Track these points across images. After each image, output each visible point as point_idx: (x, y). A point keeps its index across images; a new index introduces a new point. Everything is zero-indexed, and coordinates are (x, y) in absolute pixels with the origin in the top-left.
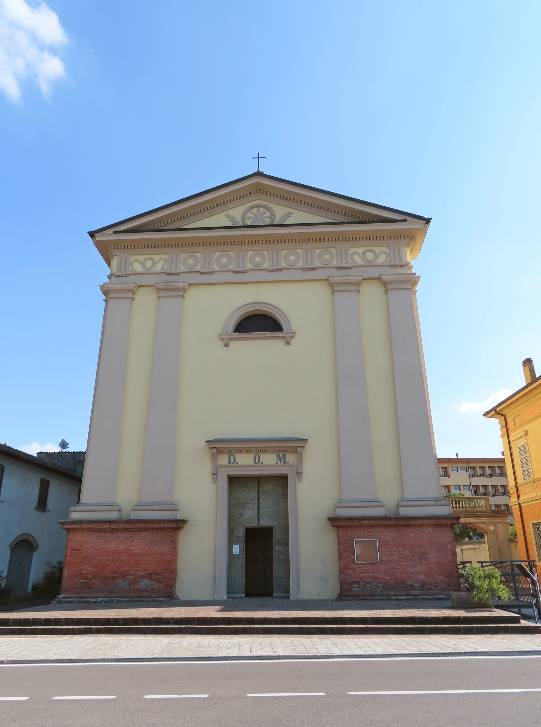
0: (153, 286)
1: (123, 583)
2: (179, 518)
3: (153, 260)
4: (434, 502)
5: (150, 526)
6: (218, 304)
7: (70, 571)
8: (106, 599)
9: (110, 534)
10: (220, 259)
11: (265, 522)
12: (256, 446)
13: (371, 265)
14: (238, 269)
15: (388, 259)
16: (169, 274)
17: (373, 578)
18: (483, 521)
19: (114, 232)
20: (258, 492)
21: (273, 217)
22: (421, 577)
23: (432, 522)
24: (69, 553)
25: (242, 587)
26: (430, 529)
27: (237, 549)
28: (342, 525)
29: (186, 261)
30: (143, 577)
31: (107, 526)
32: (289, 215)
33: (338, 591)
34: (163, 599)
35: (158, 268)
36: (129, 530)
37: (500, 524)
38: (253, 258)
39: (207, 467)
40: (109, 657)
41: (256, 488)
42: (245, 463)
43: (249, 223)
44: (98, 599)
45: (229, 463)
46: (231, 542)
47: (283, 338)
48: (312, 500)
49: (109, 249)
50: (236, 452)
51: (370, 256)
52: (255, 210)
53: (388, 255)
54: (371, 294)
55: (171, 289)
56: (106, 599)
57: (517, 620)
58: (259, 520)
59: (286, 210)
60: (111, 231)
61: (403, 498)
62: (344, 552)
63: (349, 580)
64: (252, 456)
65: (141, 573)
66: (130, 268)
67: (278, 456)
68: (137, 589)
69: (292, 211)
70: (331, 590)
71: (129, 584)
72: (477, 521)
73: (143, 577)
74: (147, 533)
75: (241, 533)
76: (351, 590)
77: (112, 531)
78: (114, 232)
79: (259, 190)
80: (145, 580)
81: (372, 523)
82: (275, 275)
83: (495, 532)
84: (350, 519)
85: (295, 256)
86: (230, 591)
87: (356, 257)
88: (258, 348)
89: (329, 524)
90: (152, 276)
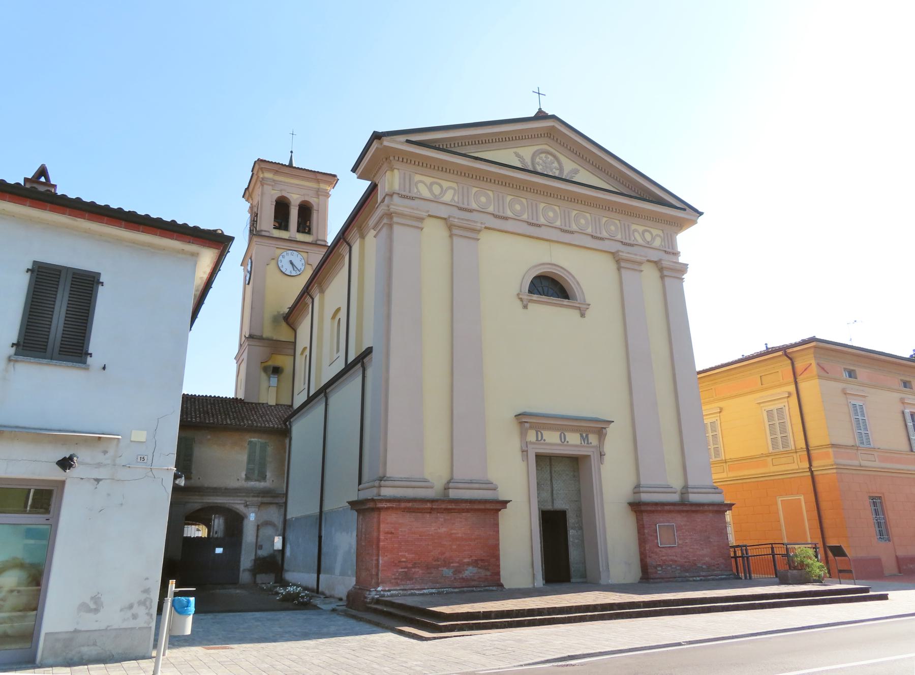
1: (447, 572)
5: (476, 507)
6: (524, 257)
7: (386, 558)
8: (434, 591)
9: (428, 515)
10: (516, 205)
11: (559, 505)
12: (564, 423)
13: (648, 246)
14: (403, 193)
15: (456, 199)
16: (460, 209)
17: (672, 560)
19: (408, 141)
20: (551, 472)
21: (561, 169)
22: (707, 559)
24: (382, 537)
26: (711, 515)
28: (638, 508)
29: (482, 198)
30: (468, 564)
31: (429, 505)
33: (640, 575)
34: (494, 588)
35: (447, 197)
36: (448, 511)
38: (550, 213)
39: (515, 443)
41: (548, 468)
42: (552, 441)
43: (539, 169)
44: (425, 591)
45: (537, 440)
49: (392, 158)
50: (544, 429)
54: (650, 275)
55: (461, 228)
56: (434, 591)
57: (866, 590)
58: (553, 503)
59: (575, 166)
60: (403, 138)
61: (452, 478)
62: (643, 537)
63: (654, 564)
64: (558, 433)
65: (466, 560)
66: (416, 190)
67: (581, 436)
68: (463, 578)
70: (633, 574)
71: (455, 573)
73: (468, 564)
74: (469, 515)
76: (656, 573)
77: (431, 511)
78: (408, 141)
80: (471, 568)
82: (566, 236)
84: (656, 504)
85: (583, 220)
87: (421, 187)
88: (548, 314)
89: (629, 509)
90: (443, 207)
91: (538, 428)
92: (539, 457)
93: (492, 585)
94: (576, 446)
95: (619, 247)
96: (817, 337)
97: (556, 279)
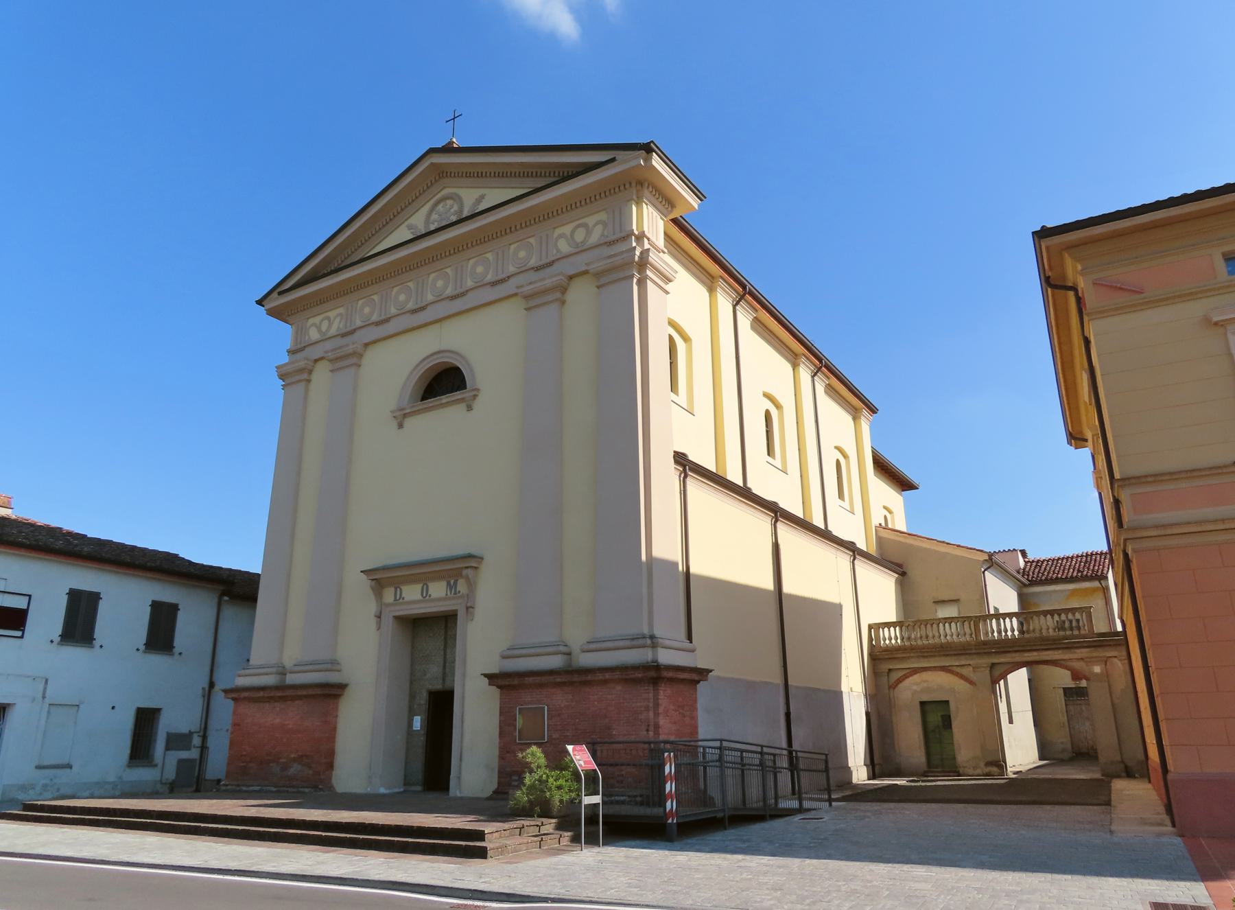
0: (516, 295)
2: (701, 665)
3: (585, 225)
4: (628, 643)
6: (396, 364)
18: (1079, 656)
20: (445, 638)
23: (617, 675)
25: (420, 776)
26: (619, 688)
27: (417, 723)
29: (365, 308)
31: (261, 694)
32: (482, 197)
33: (494, 786)
37: (1115, 660)
40: (377, 878)
42: (413, 598)
46: (411, 713)
47: (462, 400)
48: (481, 649)
51: (580, 235)
52: (440, 207)
53: (605, 224)
55: (347, 359)
58: (444, 680)
59: (475, 193)
60: (275, 294)
67: (448, 583)
69: (482, 191)
72: (1066, 657)
73: (294, 760)
75: (423, 699)
78: (280, 293)
79: (441, 173)
81: (538, 679)
83: (1106, 676)
86: (407, 783)
88: (446, 418)
91: (397, 583)
92: (401, 620)
93: (314, 782)
94: (440, 599)
95: (340, 342)
96: (1050, 224)
97: (434, 374)
